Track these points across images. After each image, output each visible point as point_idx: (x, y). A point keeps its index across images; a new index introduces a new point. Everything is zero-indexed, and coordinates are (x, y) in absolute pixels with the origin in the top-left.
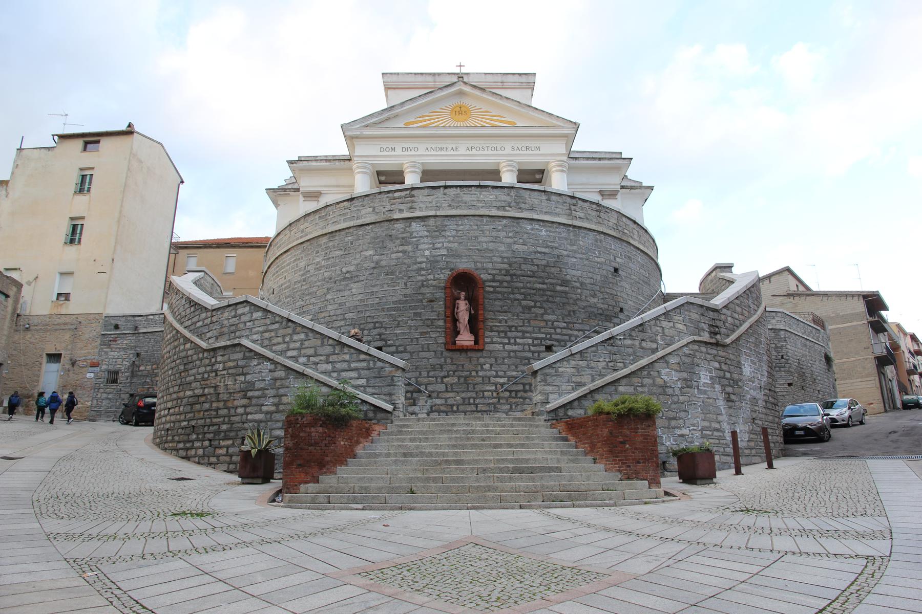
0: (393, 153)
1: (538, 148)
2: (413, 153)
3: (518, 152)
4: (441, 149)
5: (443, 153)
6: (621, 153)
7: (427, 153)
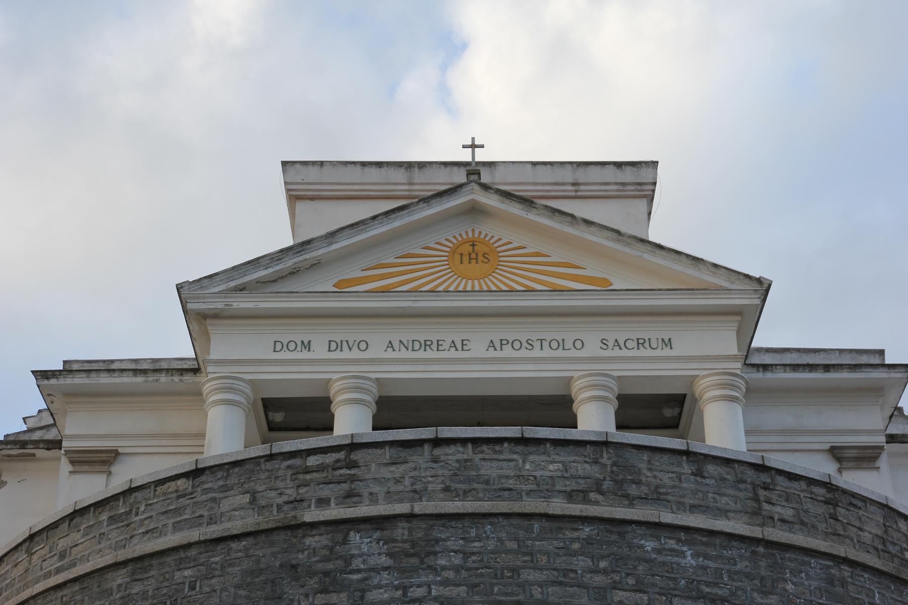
0: (305, 355)
1: (669, 343)
2: (355, 354)
3: (617, 352)
4: (426, 345)
5: (430, 354)
6: (881, 353)
7: (390, 354)
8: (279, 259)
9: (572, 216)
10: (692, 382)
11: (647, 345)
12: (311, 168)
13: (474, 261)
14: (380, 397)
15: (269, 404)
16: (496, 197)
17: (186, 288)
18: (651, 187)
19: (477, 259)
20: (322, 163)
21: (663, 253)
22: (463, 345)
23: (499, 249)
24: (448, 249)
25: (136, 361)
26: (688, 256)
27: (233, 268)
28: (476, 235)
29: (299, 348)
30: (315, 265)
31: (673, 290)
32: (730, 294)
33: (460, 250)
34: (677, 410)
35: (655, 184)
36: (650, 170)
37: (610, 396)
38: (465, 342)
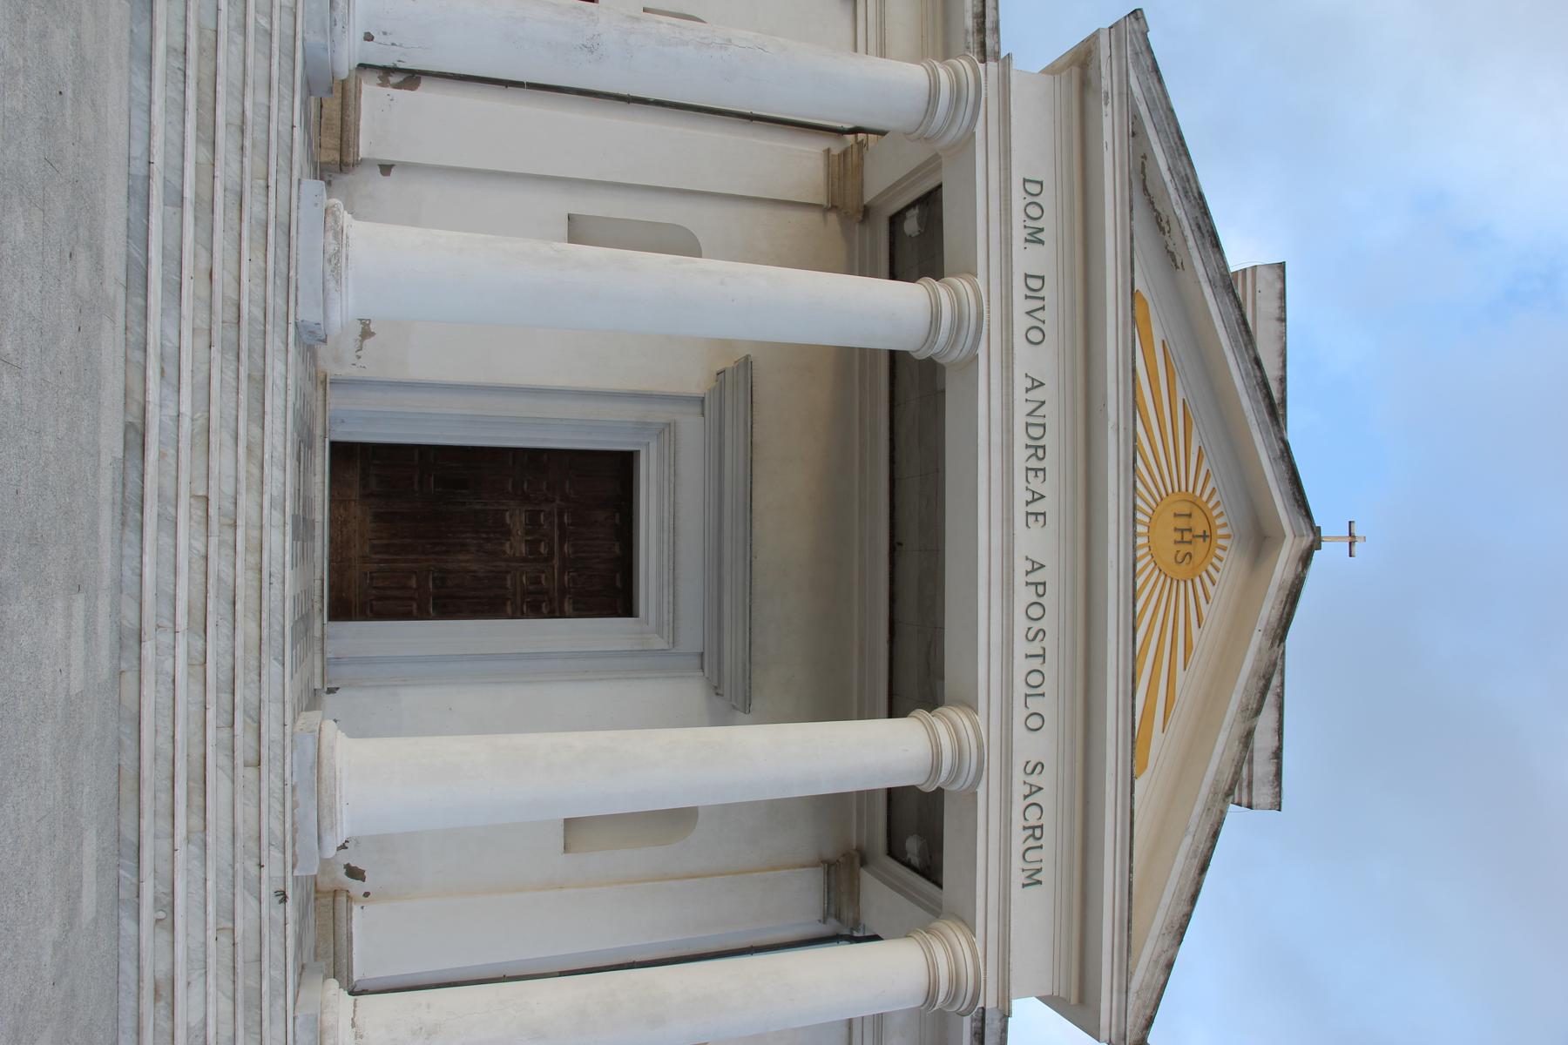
0: (1019, 234)
1: (1033, 881)
2: (1021, 322)
3: (1019, 790)
4: (1037, 450)
5: (1021, 455)
7: (1021, 384)
8: (1186, 193)
9: (1258, 711)
10: (963, 921)
11: (1031, 843)
12: (1276, 304)
13: (1178, 536)
14: (943, 368)
15: (930, 202)
16: (1289, 576)
17: (1136, 26)
18: (1245, 800)
19: (1182, 542)
20: (1283, 320)
21: (1194, 872)
22: (1036, 514)
23: (1197, 580)
24: (1198, 493)
25: (996, 29)
26: (1188, 916)
27: (1172, 111)
28: (1221, 542)
29: (1030, 223)
30: (1172, 261)
31: (1130, 893)
32: (1119, 992)
33: (1197, 513)
34: (915, 861)
35: (1250, 807)
36: (1269, 800)
37: (942, 779)
38: (1041, 518)
